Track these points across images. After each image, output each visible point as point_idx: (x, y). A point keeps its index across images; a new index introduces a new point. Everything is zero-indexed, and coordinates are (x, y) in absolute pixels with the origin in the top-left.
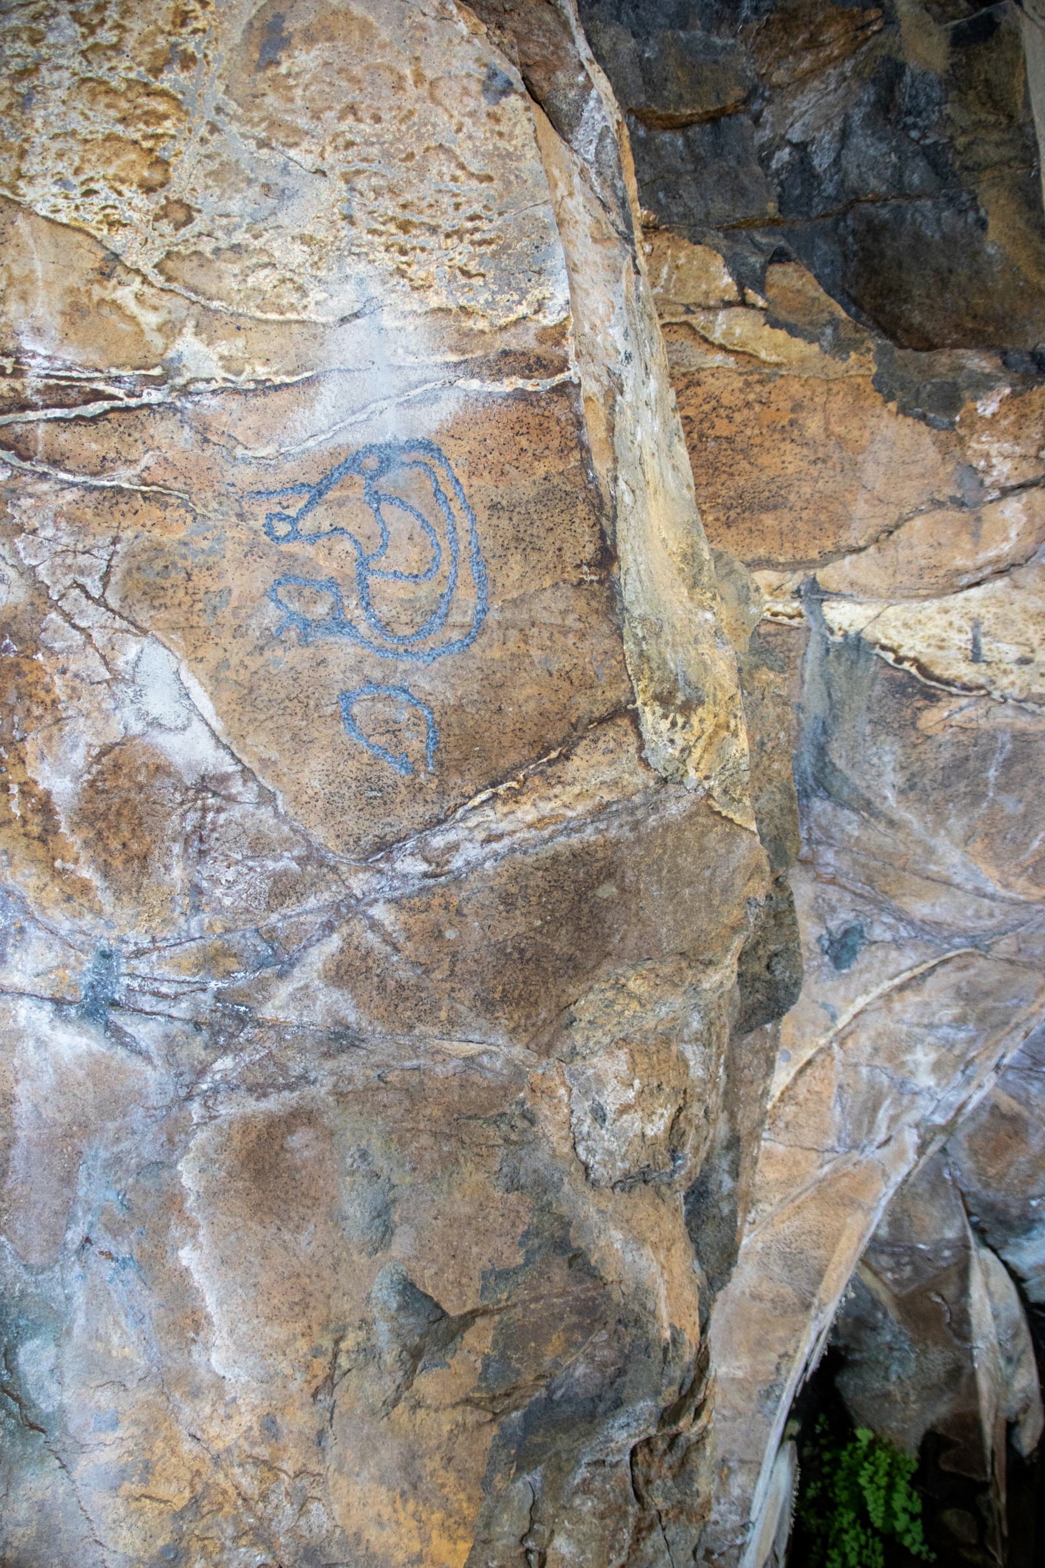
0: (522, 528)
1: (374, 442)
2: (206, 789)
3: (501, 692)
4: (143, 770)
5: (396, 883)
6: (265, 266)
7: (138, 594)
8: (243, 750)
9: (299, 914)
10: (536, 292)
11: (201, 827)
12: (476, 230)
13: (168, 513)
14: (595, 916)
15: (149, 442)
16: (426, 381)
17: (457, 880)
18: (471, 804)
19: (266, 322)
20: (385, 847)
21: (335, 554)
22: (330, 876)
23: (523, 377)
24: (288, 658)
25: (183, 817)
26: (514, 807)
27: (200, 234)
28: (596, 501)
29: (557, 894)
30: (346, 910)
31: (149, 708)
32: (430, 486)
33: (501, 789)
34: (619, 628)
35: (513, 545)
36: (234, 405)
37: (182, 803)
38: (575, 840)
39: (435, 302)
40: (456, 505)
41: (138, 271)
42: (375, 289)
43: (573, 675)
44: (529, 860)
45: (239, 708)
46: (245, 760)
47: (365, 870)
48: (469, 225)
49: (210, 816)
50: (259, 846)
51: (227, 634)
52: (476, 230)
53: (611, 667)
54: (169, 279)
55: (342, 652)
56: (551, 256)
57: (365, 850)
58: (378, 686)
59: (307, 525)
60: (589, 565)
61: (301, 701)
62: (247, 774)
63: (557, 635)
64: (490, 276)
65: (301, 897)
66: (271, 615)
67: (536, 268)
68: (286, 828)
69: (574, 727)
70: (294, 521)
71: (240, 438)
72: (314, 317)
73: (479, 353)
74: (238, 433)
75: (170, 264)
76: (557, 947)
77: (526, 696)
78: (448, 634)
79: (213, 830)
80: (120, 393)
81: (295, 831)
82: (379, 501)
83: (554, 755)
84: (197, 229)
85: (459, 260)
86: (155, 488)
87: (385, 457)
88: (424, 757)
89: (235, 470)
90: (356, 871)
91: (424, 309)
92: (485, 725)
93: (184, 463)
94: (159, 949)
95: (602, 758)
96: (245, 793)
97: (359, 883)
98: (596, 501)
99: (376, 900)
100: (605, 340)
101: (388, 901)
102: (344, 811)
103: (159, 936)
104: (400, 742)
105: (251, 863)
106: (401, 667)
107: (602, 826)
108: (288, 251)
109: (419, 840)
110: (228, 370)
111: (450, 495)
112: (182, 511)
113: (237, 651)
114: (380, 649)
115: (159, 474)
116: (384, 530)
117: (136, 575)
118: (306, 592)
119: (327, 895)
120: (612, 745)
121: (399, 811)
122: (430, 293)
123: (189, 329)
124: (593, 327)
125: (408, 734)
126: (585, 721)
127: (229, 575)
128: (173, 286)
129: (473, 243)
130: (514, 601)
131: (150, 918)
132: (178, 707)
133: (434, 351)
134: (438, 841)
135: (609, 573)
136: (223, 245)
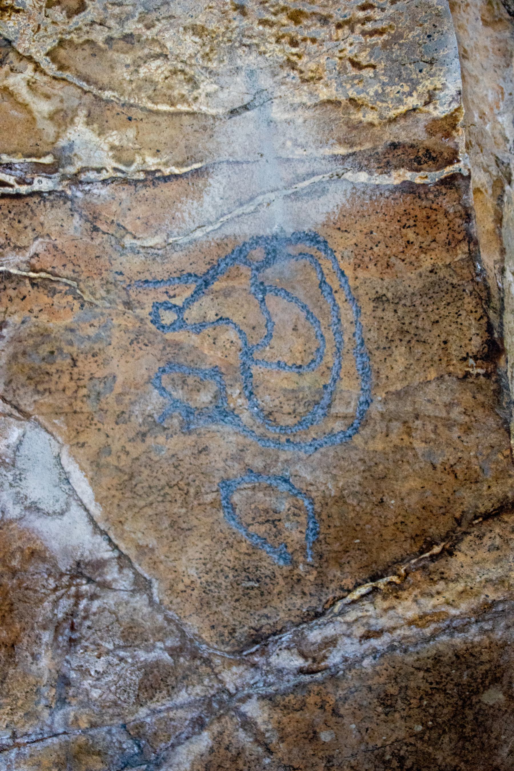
0: (407, 321)
1: (262, 233)
2: (81, 575)
3: (383, 485)
4: (18, 555)
5: (271, 678)
6: (157, 56)
7: (23, 379)
8: (121, 537)
9: (169, 709)
10: (427, 83)
11: (73, 614)
12: (368, 19)
13: (55, 299)
14: (479, 724)
15: (39, 229)
16: (314, 174)
17: (334, 677)
18: (350, 598)
19: (157, 113)
20: (260, 640)
21: (220, 343)
22: (203, 669)
23: (411, 170)
24: (170, 445)
25: (55, 603)
26: (395, 602)
27: (93, 23)
28: (484, 294)
29: (439, 698)
30: (219, 705)
31: (27, 492)
32: (316, 277)
33: (381, 583)
34: (506, 422)
35: (397, 337)
36: (123, 195)
37: (55, 589)
38: (458, 639)
39: (324, 94)
40: (340, 297)
41: (30, 59)
42: (265, 82)
43: (458, 468)
44: (409, 659)
45: (118, 494)
46: (122, 546)
47: (239, 663)
48: (361, 14)
49: (83, 603)
50: (132, 635)
51: (110, 419)
52: (368, 19)
53: (497, 462)
54: (62, 68)
55: (224, 440)
56: (443, 44)
57: (240, 642)
58: (259, 475)
59: (193, 314)
60: (475, 358)
61: (182, 488)
62: (123, 561)
63: (441, 429)
64: (381, 66)
65: (171, 690)
66: (155, 402)
67: (426, 58)
68: (160, 618)
69: (458, 522)
70: (180, 310)
71: (129, 228)
72: (204, 109)
73: (368, 146)
74: (127, 223)
75: (62, 52)
76: (439, 757)
77: (409, 488)
78: (330, 425)
79: (85, 618)
80: (11, 180)
81: (169, 620)
82: (264, 292)
83: (437, 550)
84: (89, 18)
85: (350, 51)
86: (43, 275)
87: (272, 248)
88: (303, 548)
89: (123, 259)
90: (230, 665)
91: (314, 101)
92: (366, 518)
93: (73, 250)
94: (18, 746)
95: (487, 555)
96: (121, 580)
97: (232, 677)
98: (484, 294)
99: (249, 696)
100: (493, 128)
101: (262, 697)
102: (220, 601)
103: (20, 731)
104: (279, 532)
105: (122, 654)
106: (283, 456)
107: (487, 626)
108: (180, 42)
109: (295, 634)
110: (119, 160)
111: (335, 287)
112: (70, 298)
113: (119, 437)
114: (262, 438)
115: (48, 261)
116: (269, 320)
117: (21, 360)
118: (190, 381)
119: (198, 689)
120: (498, 541)
121: (276, 602)
122: (320, 85)
123: (80, 119)
124: (482, 116)
125: (287, 525)
126: (470, 516)
127: (115, 362)
128: (66, 74)
129: (364, 33)
130: (398, 393)
131: (13, 712)
132: (57, 492)
133: (323, 143)
134: (315, 635)
135: (496, 367)
136: (116, 34)
